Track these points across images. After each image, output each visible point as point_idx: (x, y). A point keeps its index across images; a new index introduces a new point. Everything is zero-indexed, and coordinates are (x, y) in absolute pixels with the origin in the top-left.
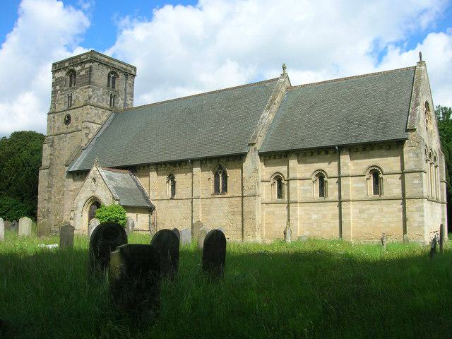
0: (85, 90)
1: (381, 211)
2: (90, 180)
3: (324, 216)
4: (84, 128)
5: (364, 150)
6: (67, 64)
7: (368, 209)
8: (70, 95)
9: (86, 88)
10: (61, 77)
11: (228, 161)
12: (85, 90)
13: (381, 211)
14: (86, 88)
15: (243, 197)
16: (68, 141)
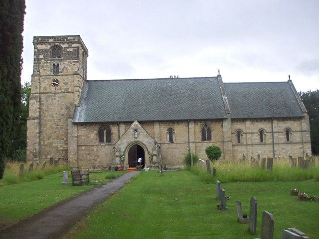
0: (73, 63)
1: (292, 148)
2: (132, 130)
3: (265, 152)
4: (76, 91)
5: (283, 120)
6: (51, 40)
7: (286, 148)
8: (56, 64)
9: (74, 62)
10: (45, 50)
11: (212, 122)
12: (73, 63)
13: (292, 148)
14: (74, 62)
15: (273, 144)
16: (57, 99)
